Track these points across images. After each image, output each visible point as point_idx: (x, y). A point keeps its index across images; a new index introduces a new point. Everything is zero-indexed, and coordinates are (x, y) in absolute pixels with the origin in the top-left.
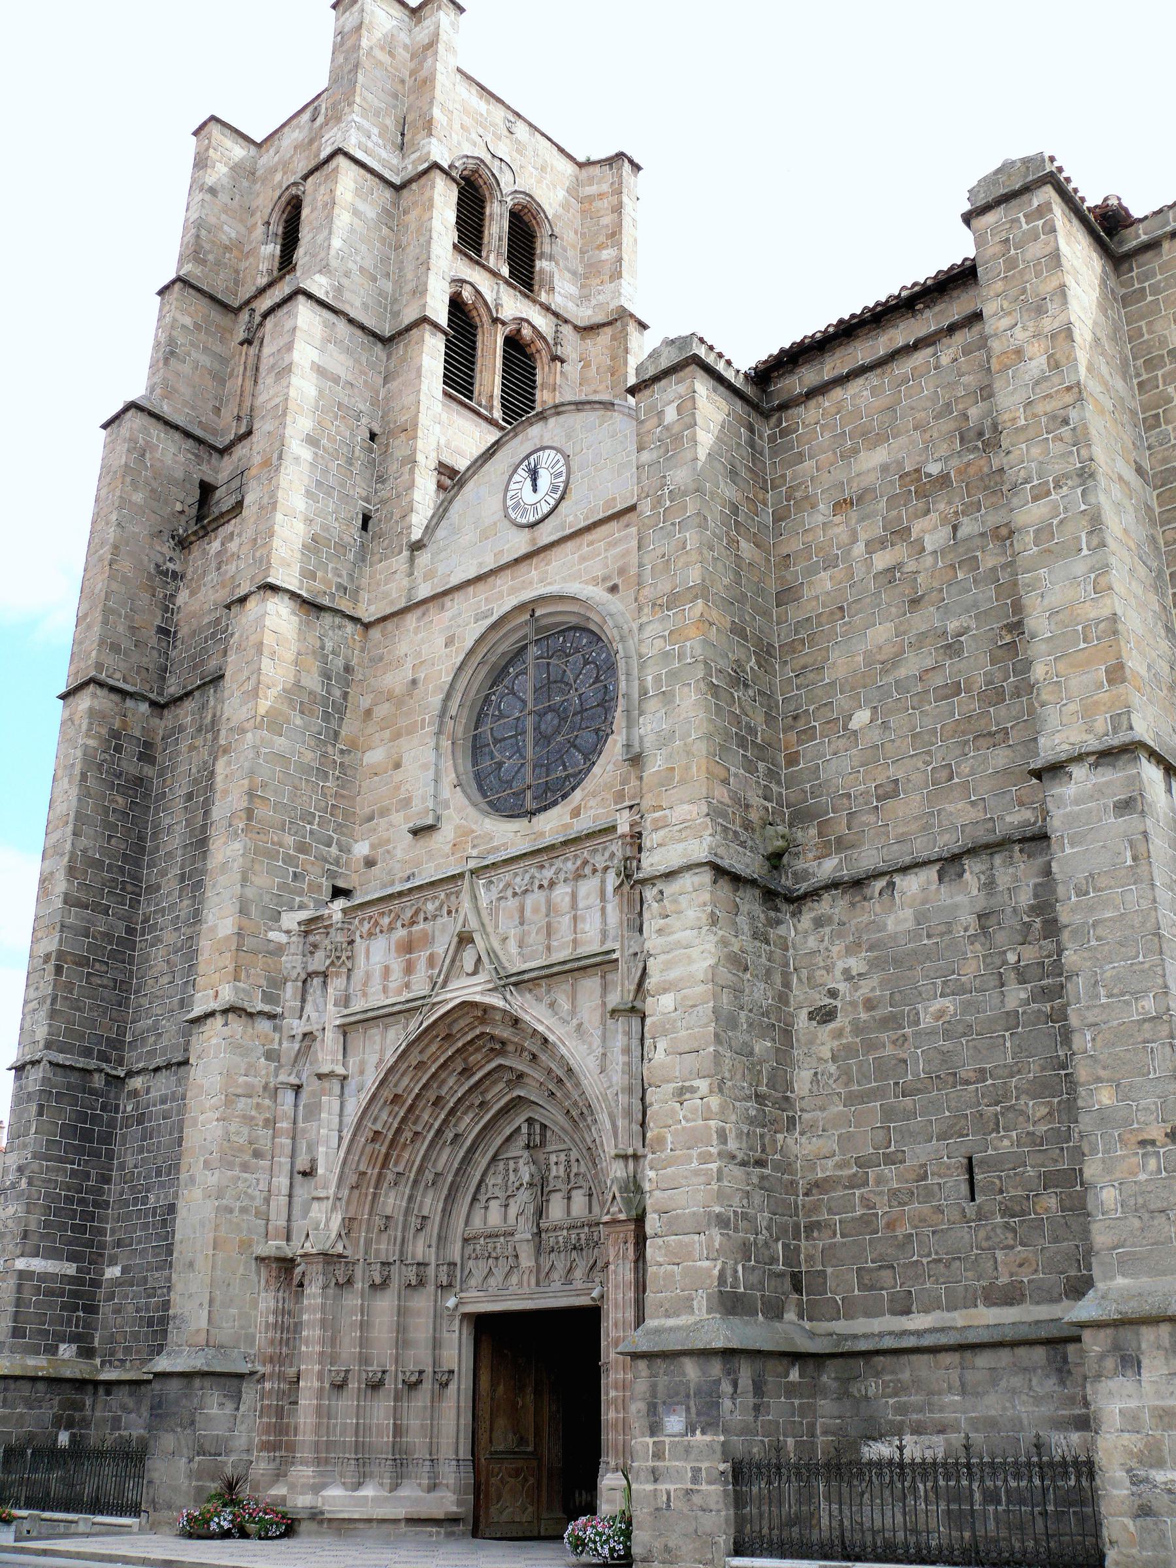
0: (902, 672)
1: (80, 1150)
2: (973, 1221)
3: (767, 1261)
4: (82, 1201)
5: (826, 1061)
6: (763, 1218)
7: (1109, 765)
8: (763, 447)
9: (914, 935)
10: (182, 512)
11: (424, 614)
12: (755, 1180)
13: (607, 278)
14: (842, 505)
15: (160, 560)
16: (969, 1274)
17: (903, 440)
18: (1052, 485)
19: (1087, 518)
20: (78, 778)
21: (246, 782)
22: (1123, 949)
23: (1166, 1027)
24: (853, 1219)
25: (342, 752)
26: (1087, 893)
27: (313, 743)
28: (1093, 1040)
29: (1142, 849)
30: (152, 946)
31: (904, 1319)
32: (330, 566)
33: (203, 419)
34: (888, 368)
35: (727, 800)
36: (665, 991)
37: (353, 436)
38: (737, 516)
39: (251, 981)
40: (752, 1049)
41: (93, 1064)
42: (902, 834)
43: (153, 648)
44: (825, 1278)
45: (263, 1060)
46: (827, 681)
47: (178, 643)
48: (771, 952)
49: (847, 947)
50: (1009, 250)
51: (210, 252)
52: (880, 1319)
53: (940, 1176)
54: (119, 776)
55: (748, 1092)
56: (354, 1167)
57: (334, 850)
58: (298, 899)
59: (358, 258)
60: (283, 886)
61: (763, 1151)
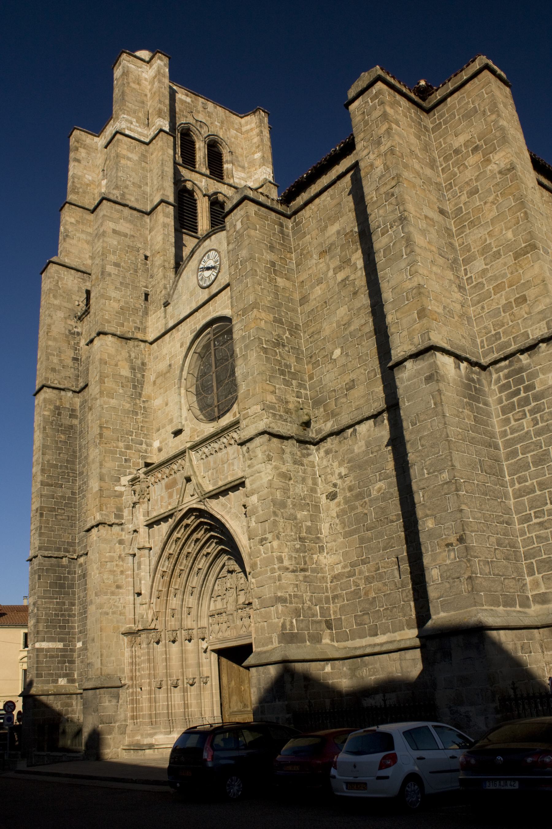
0: (352, 328)
1: (60, 593)
2: (400, 588)
3: (310, 616)
4: (63, 615)
5: (335, 518)
6: (307, 596)
7: (421, 359)
8: (289, 233)
9: (366, 453)
10: (79, 305)
11: (171, 334)
12: (301, 578)
13: (258, 167)
14: (322, 254)
15: (71, 328)
16: (400, 614)
17: (345, 218)
18: (389, 227)
19: (405, 239)
20: (42, 429)
21: (98, 422)
22: (433, 450)
23: (454, 486)
24: (351, 592)
25: (144, 402)
26: (416, 424)
27: (129, 400)
28: (423, 496)
29: (438, 399)
30: (83, 499)
31: (375, 638)
32: (131, 319)
33: (85, 263)
34: (336, 185)
35: (274, 401)
36: (253, 494)
37: (136, 259)
38: (275, 267)
39: (108, 510)
40: (296, 516)
41: (62, 554)
42: (358, 405)
43: (71, 367)
44: (342, 622)
45: (117, 544)
46: (322, 337)
47: (82, 363)
48: (305, 469)
49: (339, 463)
50: (365, 117)
51: (81, 188)
52: (365, 639)
53: (385, 568)
54: (61, 426)
55: (294, 537)
56: (156, 588)
57: (144, 446)
58: (128, 470)
59: (131, 179)
60: (120, 466)
61: (305, 563)
